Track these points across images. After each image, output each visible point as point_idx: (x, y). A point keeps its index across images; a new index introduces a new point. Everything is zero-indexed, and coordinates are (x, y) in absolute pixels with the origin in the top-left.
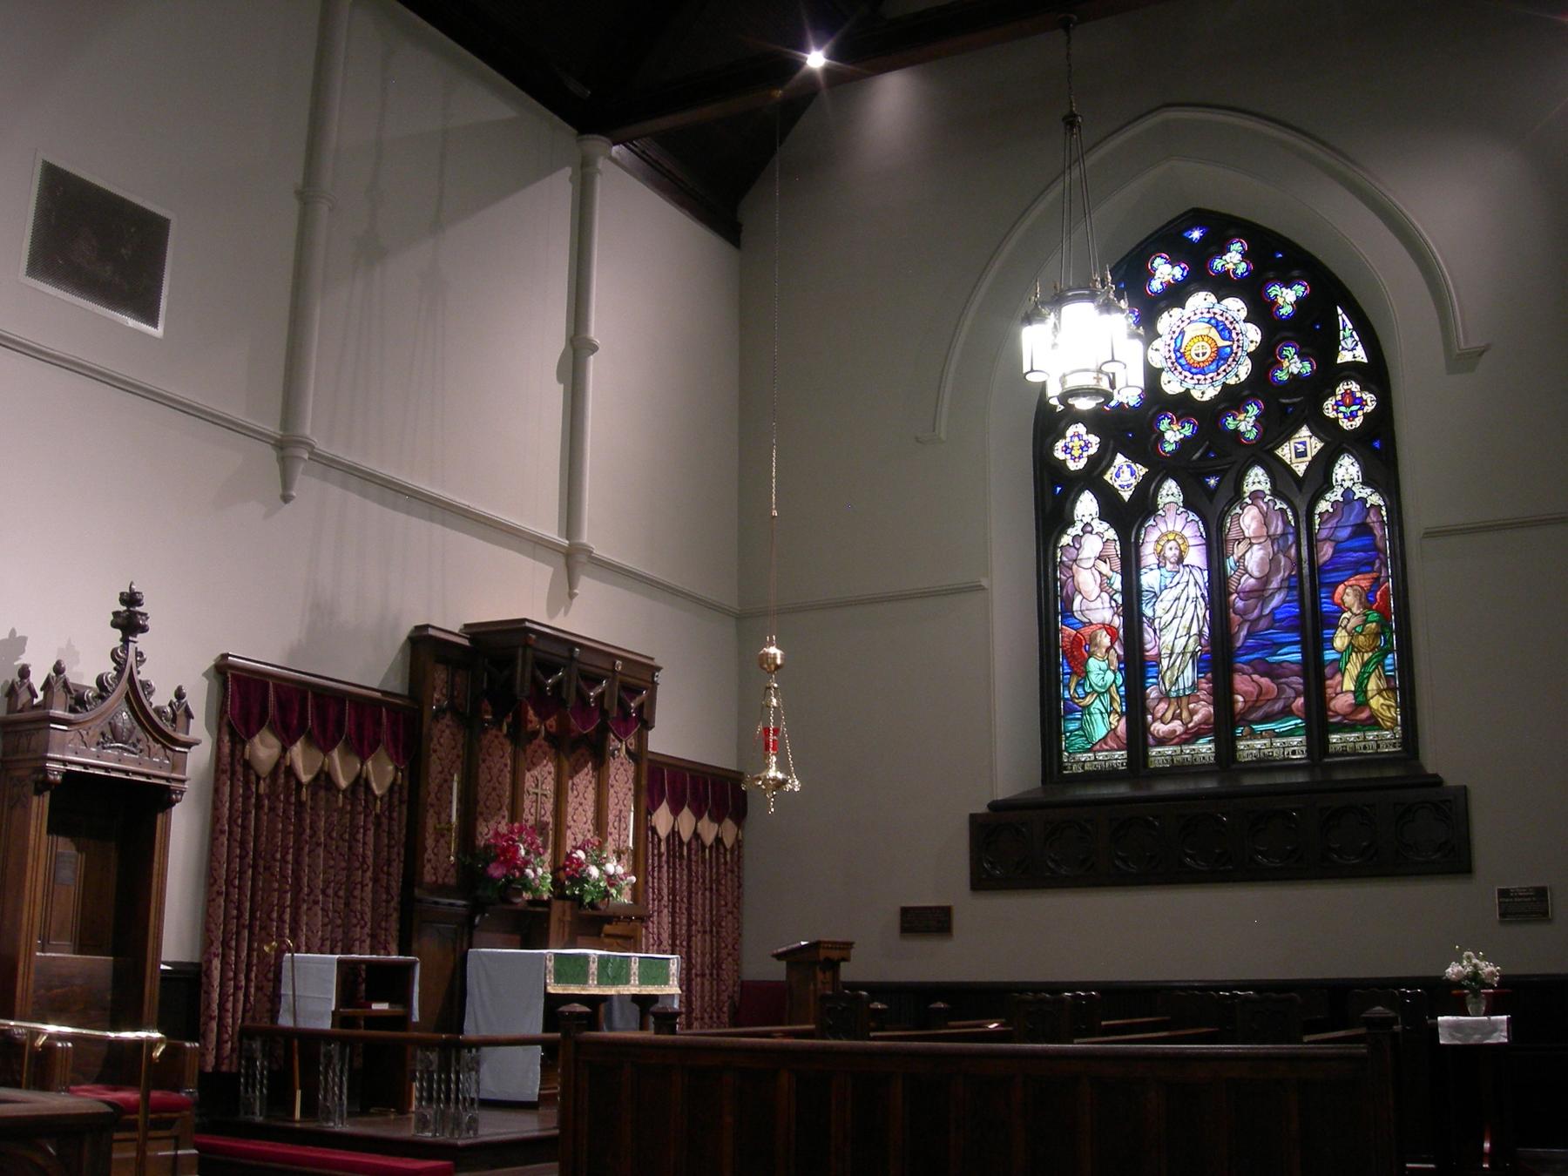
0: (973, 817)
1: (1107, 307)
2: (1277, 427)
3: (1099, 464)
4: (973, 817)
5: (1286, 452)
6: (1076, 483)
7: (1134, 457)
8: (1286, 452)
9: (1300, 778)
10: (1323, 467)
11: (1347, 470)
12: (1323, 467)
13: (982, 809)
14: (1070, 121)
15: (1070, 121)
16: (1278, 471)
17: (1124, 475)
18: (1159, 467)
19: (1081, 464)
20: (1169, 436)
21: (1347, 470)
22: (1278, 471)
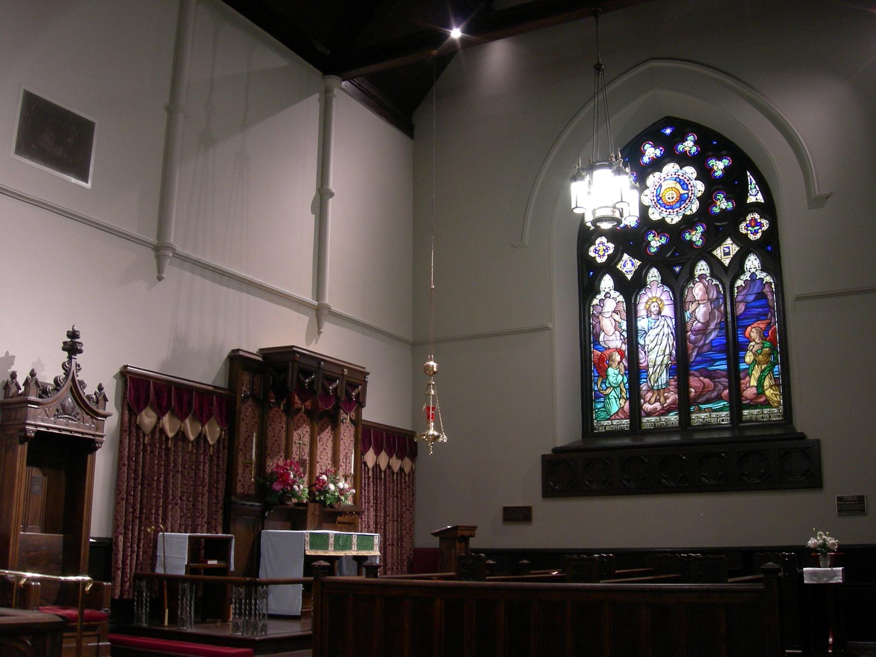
0: (543, 456)
1: (618, 172)
2: (713, 238)
3: (614, 259)
4: (543, 456)
5: (718, 253)
6: (601, 270)
7: (633, 255)
8: (718, 253)
9: (726, 435)
10: (739, 261)
11: (752, 263)
12: (739, 261)
13: (549, 452)
14: (598, 68)
15: (598, 68)
16: (714, 263)
17: (628, 265)
18: (648, 261)
19: (604, 259)
20: (653, 244)
21: (752, 263)
22: (714, 263)
